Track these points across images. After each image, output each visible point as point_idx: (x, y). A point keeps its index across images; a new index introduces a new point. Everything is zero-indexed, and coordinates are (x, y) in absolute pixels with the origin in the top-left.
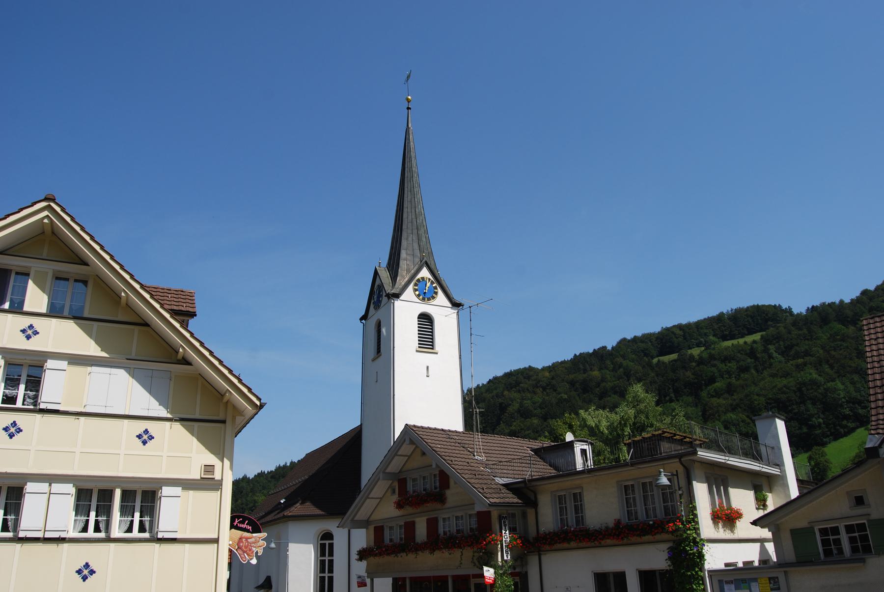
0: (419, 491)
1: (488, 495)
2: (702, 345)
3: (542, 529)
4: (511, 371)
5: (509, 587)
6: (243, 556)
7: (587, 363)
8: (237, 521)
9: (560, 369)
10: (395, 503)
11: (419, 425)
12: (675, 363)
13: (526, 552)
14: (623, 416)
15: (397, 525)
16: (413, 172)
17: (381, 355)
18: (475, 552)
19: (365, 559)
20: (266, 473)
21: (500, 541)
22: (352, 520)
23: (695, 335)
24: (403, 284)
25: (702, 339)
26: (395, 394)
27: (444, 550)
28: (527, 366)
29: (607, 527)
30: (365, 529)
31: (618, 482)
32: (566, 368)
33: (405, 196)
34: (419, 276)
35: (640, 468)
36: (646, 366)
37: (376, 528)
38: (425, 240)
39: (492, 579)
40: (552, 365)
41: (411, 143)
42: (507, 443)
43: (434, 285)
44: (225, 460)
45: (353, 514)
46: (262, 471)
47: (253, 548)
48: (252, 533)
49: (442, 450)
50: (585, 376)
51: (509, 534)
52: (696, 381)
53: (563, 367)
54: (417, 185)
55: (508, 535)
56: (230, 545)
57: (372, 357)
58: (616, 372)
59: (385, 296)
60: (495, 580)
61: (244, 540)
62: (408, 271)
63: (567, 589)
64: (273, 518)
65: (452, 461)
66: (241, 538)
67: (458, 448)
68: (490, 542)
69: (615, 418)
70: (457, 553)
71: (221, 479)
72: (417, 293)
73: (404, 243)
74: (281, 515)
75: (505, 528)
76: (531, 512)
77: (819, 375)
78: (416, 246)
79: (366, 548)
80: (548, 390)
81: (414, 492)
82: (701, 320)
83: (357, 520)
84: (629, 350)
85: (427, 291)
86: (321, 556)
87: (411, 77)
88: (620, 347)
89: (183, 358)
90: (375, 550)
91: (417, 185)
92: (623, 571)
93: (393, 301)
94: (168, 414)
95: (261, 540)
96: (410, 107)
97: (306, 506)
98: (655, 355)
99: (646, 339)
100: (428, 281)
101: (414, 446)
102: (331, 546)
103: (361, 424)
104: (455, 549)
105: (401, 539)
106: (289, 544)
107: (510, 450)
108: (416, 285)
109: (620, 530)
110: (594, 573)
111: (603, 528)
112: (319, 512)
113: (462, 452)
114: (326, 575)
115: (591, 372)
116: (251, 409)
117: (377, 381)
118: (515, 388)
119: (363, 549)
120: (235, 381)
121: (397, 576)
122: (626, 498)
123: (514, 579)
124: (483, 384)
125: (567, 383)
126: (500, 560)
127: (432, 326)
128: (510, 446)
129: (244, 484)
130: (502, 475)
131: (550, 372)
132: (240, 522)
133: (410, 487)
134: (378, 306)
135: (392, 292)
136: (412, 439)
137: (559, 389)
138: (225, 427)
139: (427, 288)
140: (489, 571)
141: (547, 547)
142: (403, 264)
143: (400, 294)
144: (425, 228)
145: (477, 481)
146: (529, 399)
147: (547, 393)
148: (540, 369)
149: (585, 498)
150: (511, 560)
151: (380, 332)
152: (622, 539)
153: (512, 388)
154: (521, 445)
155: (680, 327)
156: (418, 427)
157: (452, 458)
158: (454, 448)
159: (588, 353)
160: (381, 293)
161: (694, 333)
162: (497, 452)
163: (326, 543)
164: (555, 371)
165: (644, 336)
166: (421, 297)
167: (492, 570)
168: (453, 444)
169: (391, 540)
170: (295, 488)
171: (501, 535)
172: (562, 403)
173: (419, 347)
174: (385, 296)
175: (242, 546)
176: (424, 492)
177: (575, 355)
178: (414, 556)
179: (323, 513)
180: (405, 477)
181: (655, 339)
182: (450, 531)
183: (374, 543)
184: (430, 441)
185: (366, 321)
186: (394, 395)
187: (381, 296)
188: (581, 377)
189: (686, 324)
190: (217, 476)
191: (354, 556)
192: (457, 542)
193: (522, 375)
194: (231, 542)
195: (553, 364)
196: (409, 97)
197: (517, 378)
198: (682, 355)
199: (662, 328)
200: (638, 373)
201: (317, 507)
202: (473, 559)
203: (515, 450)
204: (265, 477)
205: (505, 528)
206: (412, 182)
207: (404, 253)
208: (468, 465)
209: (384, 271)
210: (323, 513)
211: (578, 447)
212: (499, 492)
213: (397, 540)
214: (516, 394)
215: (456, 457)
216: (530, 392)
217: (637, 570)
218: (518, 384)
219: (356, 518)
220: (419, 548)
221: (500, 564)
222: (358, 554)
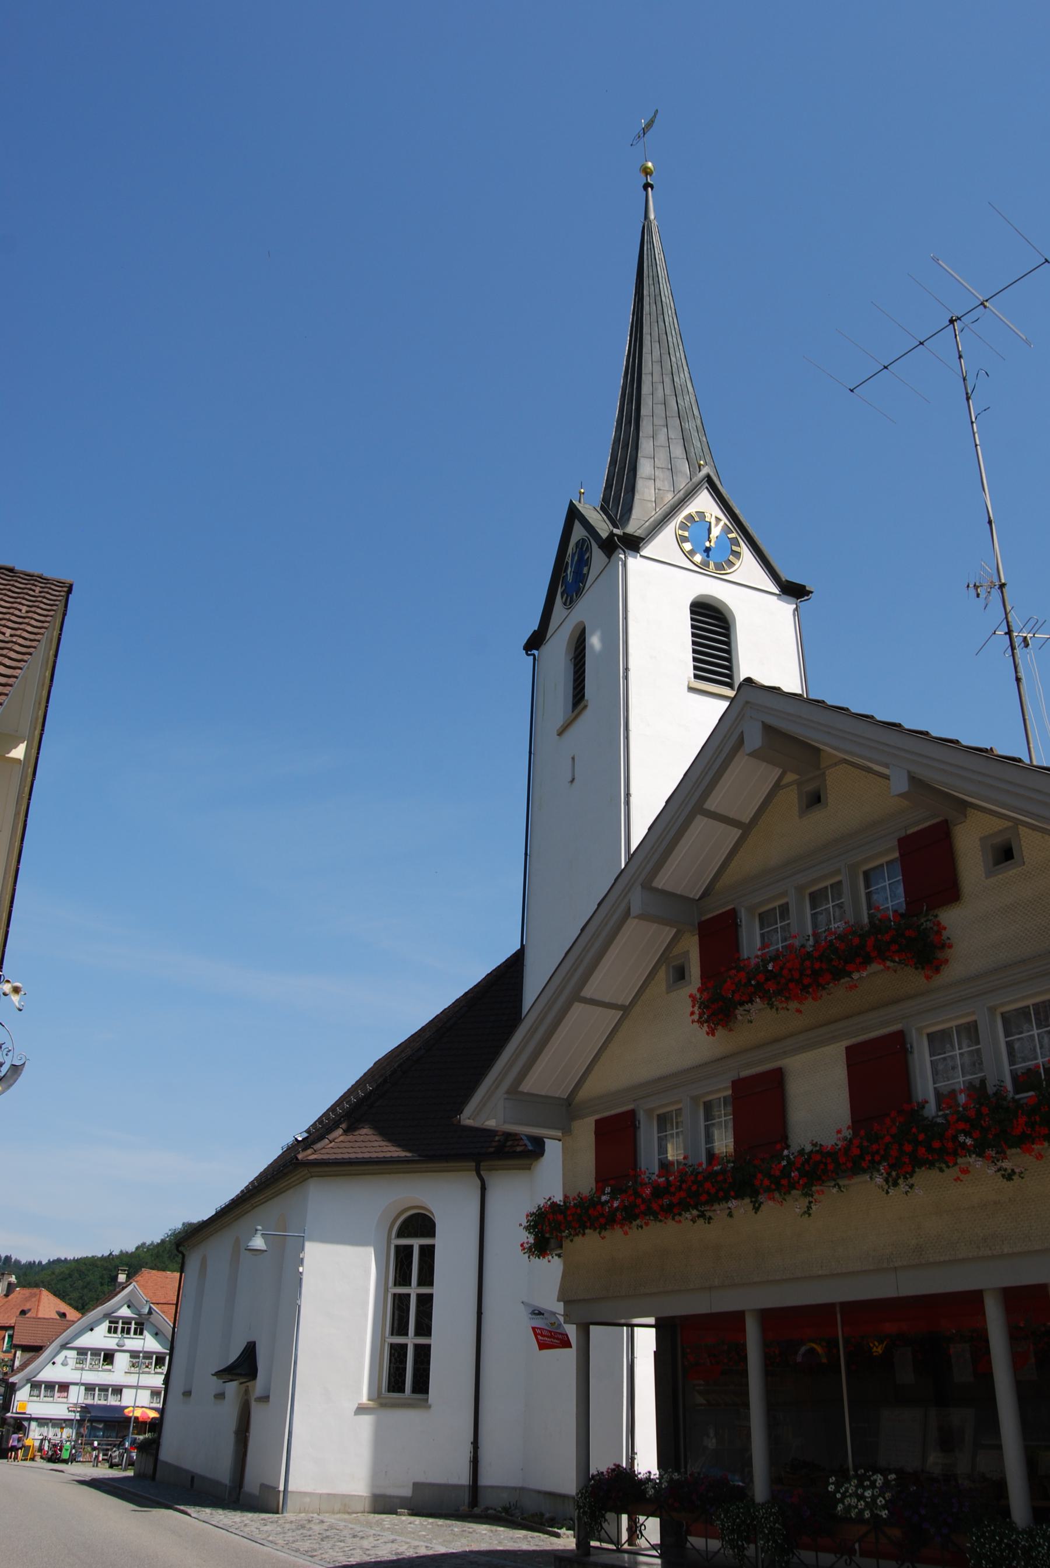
15: (695, 1099)
17: (586, 707)
26: (632, 791)
33: (646, 349)
34: (691, 509)
38: (699, 445)
57: (559, 721)
72: (688, 546)
73: (646, 446)
77: (514, 1542)
78: (678, 451)
86: (397, 1283)
87: (655, 124)
93: (622, 556)
97: (362, 1138)
102: (428, 1253)
103: (522, 945)
108: (683, 526)
114: (411, 1340)
127: (728, 636)
163: (411, 1247)
179: (409, 1154)
196: (650, 165)
201: (389, 1140)
206: (661, 323)
210: (403, 1154)
219: (526, 1087)
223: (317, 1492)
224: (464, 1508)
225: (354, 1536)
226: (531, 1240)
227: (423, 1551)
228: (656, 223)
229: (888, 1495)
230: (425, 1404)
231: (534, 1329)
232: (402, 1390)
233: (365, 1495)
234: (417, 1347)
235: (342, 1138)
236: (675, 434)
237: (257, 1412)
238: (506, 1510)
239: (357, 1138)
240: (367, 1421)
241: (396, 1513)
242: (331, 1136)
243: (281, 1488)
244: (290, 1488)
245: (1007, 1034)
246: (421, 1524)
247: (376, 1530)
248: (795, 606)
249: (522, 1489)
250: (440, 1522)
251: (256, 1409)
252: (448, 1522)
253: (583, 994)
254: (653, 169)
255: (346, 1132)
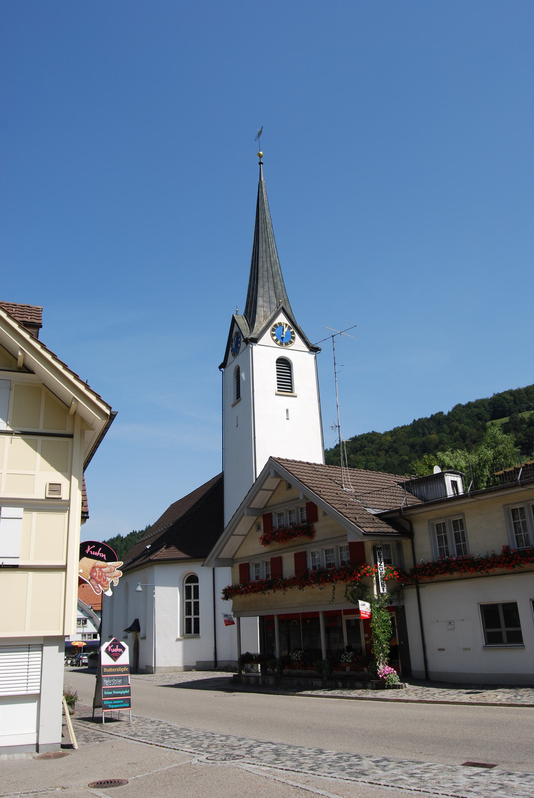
0: (285, 525)
1: (362, 525)
2: (531, 409)
3: (420, 560)
4: (356, 436)
5: (386, 622)
6: (97, 587)
7: (426, 427)
8: (89, 549)
9: (401, 433)
10: (261, 538)
11: (284, 458)
12: (507, 425)
13: (403, 585)
14: (482, 457)
15: (263, 561)
16: (267, 223)
17: (241, 400)
18: (349, 585)
19: (231, 598)
20: (137, 532)
21: (376, 574)
22: (217, 558)
23: (525, 400)
24: (261, 329)
25: (531, 404)
27: (314, 585)
28: (371, 431)
29: (493, 555)
30: (230, 567)
31: (505, 505)
32: (406, 433)
33: (260, 246)
34: (276, 322)
35: (530, 489)
36: (480, 428)
37: (241, 566)
38: (281, 288)
39: (369, 614)
40: (394, 430)
41: (265, 196)
42: (374, 477)
43: (291, 330)
44: (73, 478)
45: (217, 553)
46: (133, 531)
47: (107, 578)
48: (106, 561)
49: (309, 481)
50: (424, 439)
51: (385, 566)
52: (527, 441)
53: (404, 431)
54: (271, 236)
55: (383, 567)
56: (80, 573)
58: (453, 435)
59: (243, 341)
60: (371, 615)
61: (97, 569)
62: (265, 317)
63: (450, 623)
64: (140, 563)
65: (320, 492)
66: (94, 568)
67: (325, 480)
68: (365, 574)
69: (474, 459)
70: (329, 588)
71: (68, 499)
72: (275, 338)
73: (260, 291)
74: (147, 559)
75: (380, 560)
76: (406, 543)
78: (272, 293)
79: (232, 586)
80: (390, 453)
81: (280, 527)
82: (530, 386)
83: (221, 558)
84: (464, 415)
85: (284, 336)
86: (187, 598)
88: (455, 412)
89: (24, 365)
90: (241, 587)
91: (271, 236)
92: (515, 601)
93: (251, 346)
94: (8, 427)
95: (117, 569)
96: (261, 161)
97: (171, 551)
98: (488, 419)
99: (479, 404)
100: (285, 326)
101: (279, 480)
102: (196, 588)
104: (326, 584)
105: (268, 576)
106: (156, 587)
107: (377, 483)
108: (273, 330)
109: (510, 557)
110: (480, 605)
111: (490, 556)
112: (183, 555)
113: (330, 484)
115: (429, 435)
116: (100, 419)
117: (237, 426)
118: (360, 451)
119: (229, 587)
120: (82, 387)
121: (264, 613)
122: (514, 523)
123: (391, 613)
124: (331, 449)
125: (408, 446)
126: (375, 593)
127: (290, 370)
128: (377, 480)
129: (118, 543)
130: (374, 506)
131: (391, 437)
132: (92, 550)
133: (276, 523)
134: (236, 352)
135: (251, 336)
136: (277, 471)
137: (400, 452)
138: (73, 441)
139: (284, 333)
140: (364, 605)
141: (427, 579)
142: (260, 311)
143: (258, 339)
144: (281, 276)
145: (348, 511)
146: (373, 461)
147: (390, 455)
148: (383, 433)
149: (467, 525)
150: (387, 594)
151: (239, 378)
152: (514, 566)
153: (357, 452)
154: (388, 479)
155: (510, 393)
156: (283, 460)
157: (320, 489)
158: (320, 479)
159: (427, 418)
160: (239, 340)
161: (523, 398)
162: (365, 485)
164: (396, 436)
165: (477, 401)
166: (279, 342)
167: (368, 605)
168: (320, 476)
169: (257, 578)
170: (160, 535)
171: (377, 567)
172: (403, 464)
173: (278, 391)
174: (243, 341)
175: (96, 576)
176: (292, 526)
177: (414, 420)
178: (282, 592)
179: (188, 556)
180: (270, 512)
181: (487, 404)
182: (319, 565)
183: (240, 581)
184: (295, 472)
185: (225, 368)
186: (255, 438)
187: (240, 342)
188: (420, 440)
189: (516, 390)
190: (64, 496)
191: (220, 595)
192: (329, 575)
193: (366, 439)
194: (81, 571)
195: (395, 429)
196: (261, 153)
197: (361, 442)
198: (513, 418)
199: (494, 394)
200: (473, 435)
201: (181, 551)
202: (346, 593)
203: (382, 484)
204: (136, 536)
205: (380, 560)
206: (266, 233)
207: (261, 300)
208: (337, 496)
209: (241, 319)
211: (449, 479)
212: (373, 521)
213: (263, 576)
214: (360, 456)
215: (324, 488)
216: (374, 455)
217: (530, 600)
218: (362, 447)
219: (220, 557)
220: (286, 584)
221: (376, 597)
222: (223, 593)
223: (165, 666)
224: (213, 668)
225: (180, 677)
226: (224, 596)
227: (200, 679)
228: (264, 182)
229: (301, 655)
230: (198, 637)
231: (224, 620)
232: (190, 632)
233: (181, 666)
234: (195, 619)
235: (164, 551)
236: (271, 286)
237: (141, 643)
238: (226, 667)
239: (169, 551)
240: (180, 643)
241: (191, 671)
242: (161, 550)
243: (153, 666)
244: (156, 666)
245: (326, 554)
246: (199, 673)
247: (186, 675)
248: (315, 355)
249: (231, 661)
250: (205, 672)
251: (141, 642)
252: (208, 672)
253: (234, 534)
254: (262, 154)
255: (166, 548)
